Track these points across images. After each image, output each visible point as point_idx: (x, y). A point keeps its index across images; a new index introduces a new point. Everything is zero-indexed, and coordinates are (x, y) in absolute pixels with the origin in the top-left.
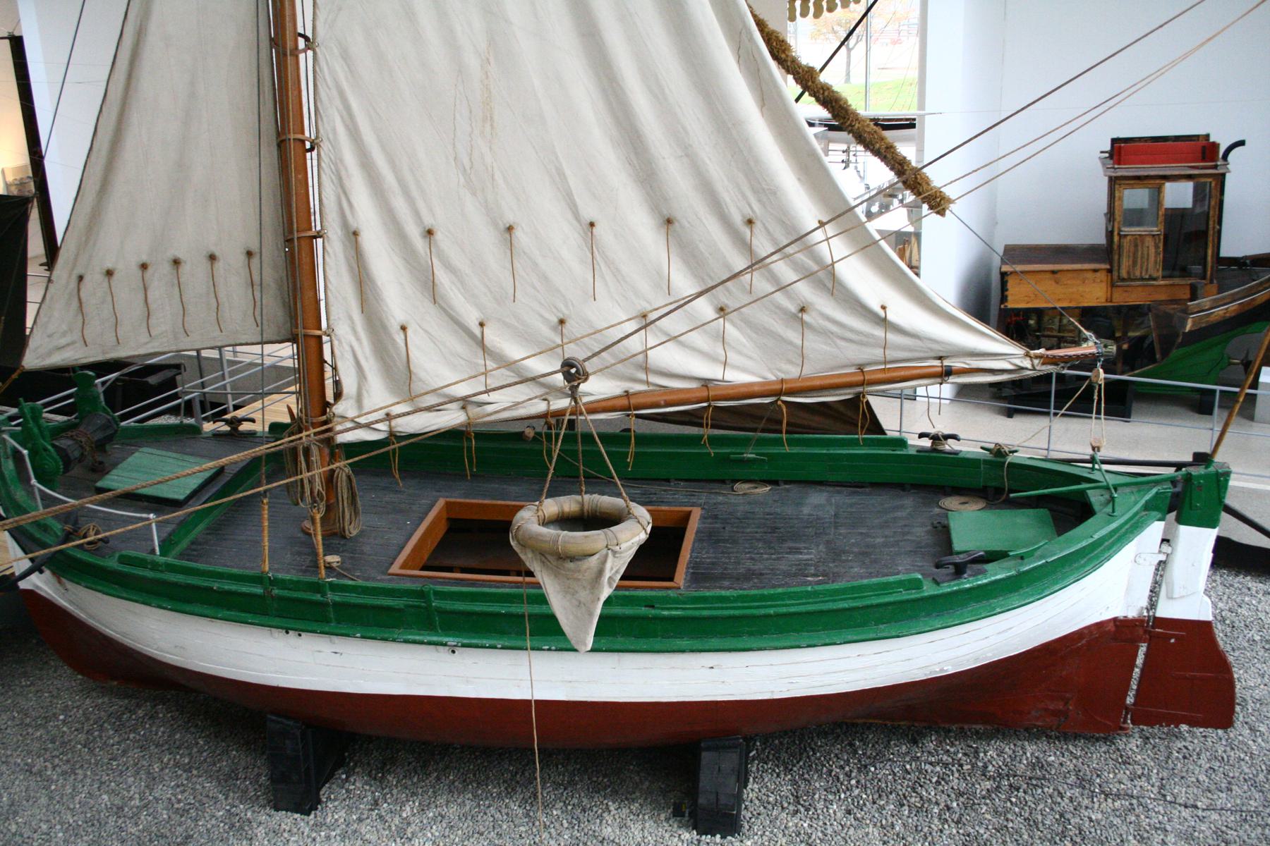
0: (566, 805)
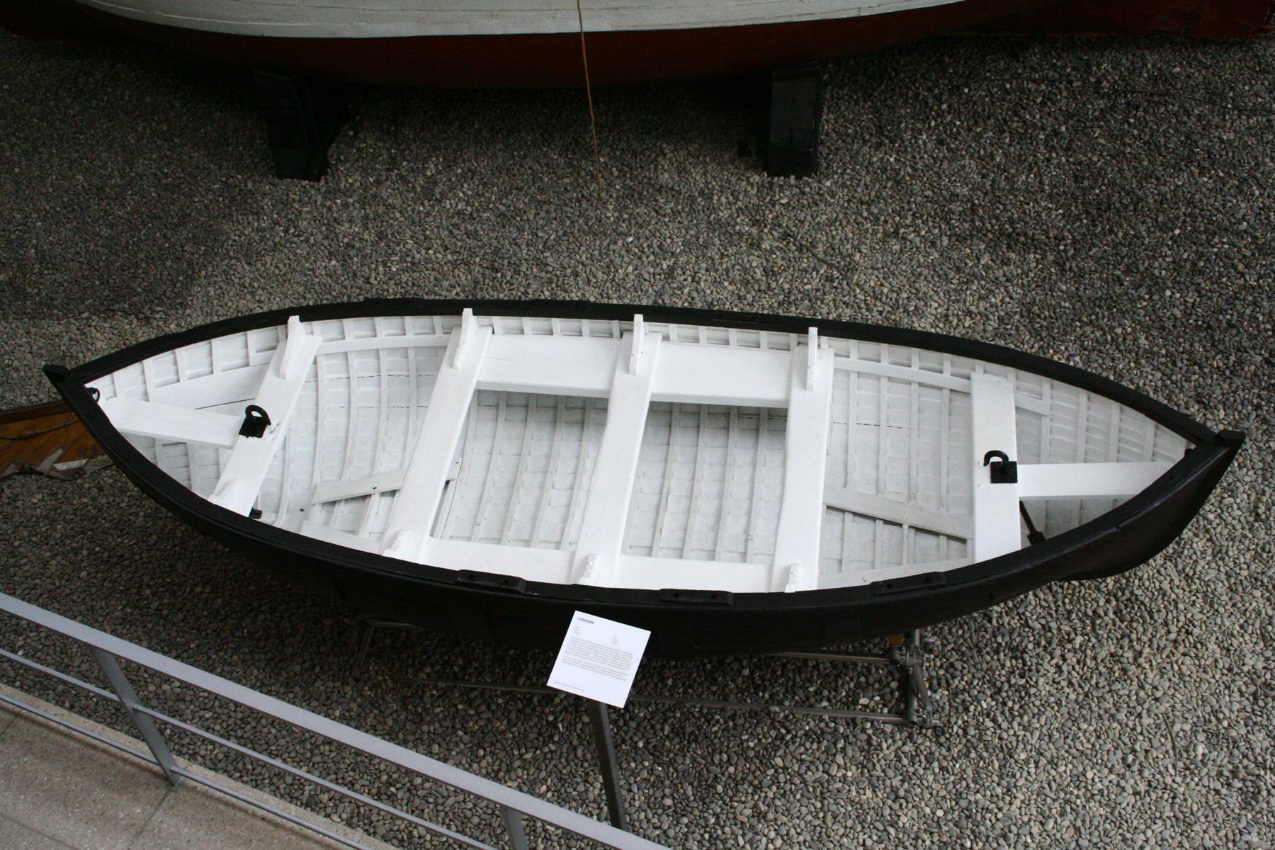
0: (614, 150)
